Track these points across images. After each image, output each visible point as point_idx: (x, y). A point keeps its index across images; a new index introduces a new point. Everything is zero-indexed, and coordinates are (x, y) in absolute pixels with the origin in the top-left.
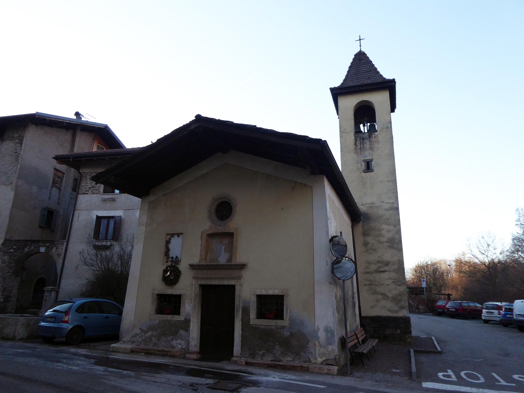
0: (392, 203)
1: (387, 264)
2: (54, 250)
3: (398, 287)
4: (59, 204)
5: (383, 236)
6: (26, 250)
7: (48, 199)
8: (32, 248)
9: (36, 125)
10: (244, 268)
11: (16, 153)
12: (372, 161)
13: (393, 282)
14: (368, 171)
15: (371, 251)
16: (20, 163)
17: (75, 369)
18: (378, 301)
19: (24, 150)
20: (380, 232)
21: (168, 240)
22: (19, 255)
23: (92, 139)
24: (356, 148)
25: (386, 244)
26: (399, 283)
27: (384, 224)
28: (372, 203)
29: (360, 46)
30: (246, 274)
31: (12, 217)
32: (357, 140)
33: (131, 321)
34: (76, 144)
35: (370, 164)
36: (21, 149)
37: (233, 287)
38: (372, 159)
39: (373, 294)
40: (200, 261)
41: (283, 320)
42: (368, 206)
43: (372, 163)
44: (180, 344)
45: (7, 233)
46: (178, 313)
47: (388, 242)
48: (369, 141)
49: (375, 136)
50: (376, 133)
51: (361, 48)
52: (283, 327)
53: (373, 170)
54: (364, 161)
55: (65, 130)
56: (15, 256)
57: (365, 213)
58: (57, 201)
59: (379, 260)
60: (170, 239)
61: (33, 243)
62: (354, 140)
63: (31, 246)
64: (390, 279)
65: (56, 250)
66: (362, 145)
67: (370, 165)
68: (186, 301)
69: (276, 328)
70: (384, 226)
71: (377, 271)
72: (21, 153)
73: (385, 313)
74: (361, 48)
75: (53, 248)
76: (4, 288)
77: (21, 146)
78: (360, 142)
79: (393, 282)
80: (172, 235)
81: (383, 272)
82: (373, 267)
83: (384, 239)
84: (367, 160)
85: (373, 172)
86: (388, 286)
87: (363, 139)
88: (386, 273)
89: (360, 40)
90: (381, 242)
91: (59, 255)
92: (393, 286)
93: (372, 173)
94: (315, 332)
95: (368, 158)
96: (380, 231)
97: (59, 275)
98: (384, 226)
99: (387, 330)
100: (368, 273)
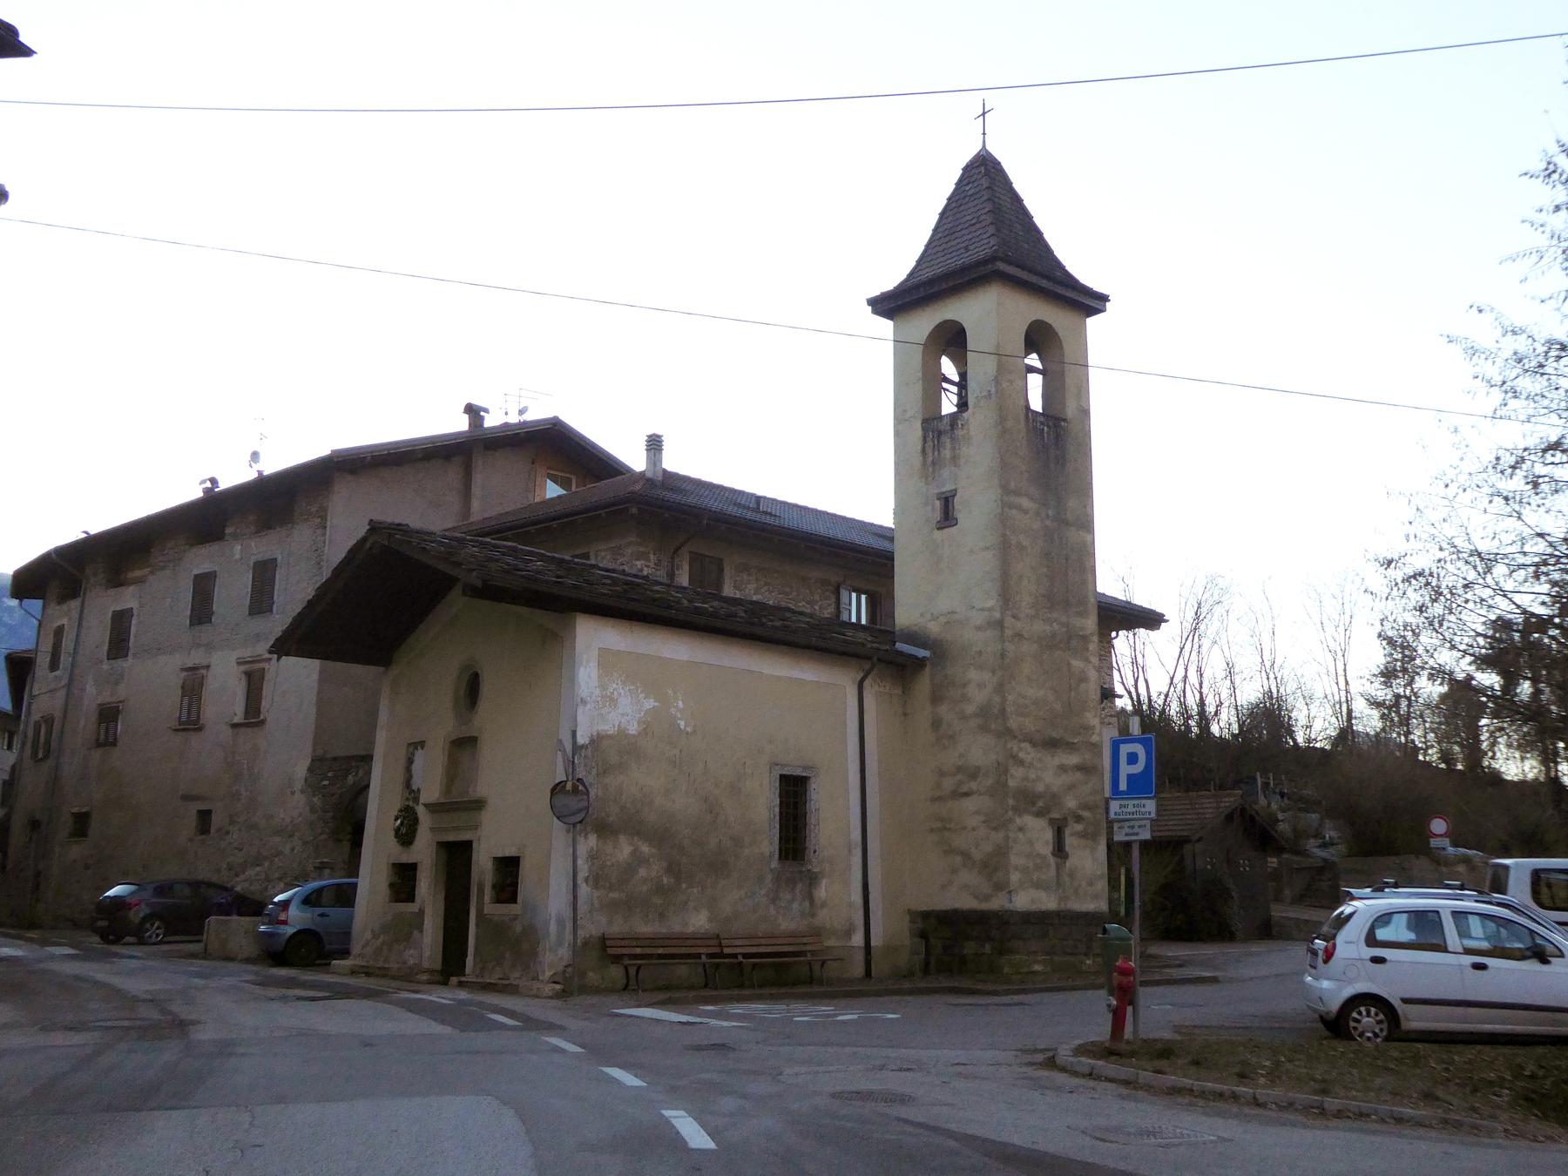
1: (974, 774)
14: (947, 523)
17: (60, 945)
18: (955, 871)
24: (924, 464)
29: (984, 134)
30: (486, 817)
31: (322, 704)
34: (476, 490)
36: (324, 543)
38: (956, 490)
39: (946, 853)
45: (316, 742)
46: (413, 901)
48: (951, 437)
51: (984, 142)
52: (516, 917)
60: (413, 754)
62: (922, 439)
63: (358, 771)
66: (936, 453)
70: (973, 675)
72: (326, 552)
73: (966, 903)
74: (984, 142)
77: (324, 534)
78: (934, 442)
79: (984, 822)
81: (966, 794)
82: (948, 784)
83: (970, 709)
85: (956, 524)
87: (940, 434)
90: (964, 718)
95: (948, 487)
96: (965, 685)
98: (973, 675)
100: (939, 799)
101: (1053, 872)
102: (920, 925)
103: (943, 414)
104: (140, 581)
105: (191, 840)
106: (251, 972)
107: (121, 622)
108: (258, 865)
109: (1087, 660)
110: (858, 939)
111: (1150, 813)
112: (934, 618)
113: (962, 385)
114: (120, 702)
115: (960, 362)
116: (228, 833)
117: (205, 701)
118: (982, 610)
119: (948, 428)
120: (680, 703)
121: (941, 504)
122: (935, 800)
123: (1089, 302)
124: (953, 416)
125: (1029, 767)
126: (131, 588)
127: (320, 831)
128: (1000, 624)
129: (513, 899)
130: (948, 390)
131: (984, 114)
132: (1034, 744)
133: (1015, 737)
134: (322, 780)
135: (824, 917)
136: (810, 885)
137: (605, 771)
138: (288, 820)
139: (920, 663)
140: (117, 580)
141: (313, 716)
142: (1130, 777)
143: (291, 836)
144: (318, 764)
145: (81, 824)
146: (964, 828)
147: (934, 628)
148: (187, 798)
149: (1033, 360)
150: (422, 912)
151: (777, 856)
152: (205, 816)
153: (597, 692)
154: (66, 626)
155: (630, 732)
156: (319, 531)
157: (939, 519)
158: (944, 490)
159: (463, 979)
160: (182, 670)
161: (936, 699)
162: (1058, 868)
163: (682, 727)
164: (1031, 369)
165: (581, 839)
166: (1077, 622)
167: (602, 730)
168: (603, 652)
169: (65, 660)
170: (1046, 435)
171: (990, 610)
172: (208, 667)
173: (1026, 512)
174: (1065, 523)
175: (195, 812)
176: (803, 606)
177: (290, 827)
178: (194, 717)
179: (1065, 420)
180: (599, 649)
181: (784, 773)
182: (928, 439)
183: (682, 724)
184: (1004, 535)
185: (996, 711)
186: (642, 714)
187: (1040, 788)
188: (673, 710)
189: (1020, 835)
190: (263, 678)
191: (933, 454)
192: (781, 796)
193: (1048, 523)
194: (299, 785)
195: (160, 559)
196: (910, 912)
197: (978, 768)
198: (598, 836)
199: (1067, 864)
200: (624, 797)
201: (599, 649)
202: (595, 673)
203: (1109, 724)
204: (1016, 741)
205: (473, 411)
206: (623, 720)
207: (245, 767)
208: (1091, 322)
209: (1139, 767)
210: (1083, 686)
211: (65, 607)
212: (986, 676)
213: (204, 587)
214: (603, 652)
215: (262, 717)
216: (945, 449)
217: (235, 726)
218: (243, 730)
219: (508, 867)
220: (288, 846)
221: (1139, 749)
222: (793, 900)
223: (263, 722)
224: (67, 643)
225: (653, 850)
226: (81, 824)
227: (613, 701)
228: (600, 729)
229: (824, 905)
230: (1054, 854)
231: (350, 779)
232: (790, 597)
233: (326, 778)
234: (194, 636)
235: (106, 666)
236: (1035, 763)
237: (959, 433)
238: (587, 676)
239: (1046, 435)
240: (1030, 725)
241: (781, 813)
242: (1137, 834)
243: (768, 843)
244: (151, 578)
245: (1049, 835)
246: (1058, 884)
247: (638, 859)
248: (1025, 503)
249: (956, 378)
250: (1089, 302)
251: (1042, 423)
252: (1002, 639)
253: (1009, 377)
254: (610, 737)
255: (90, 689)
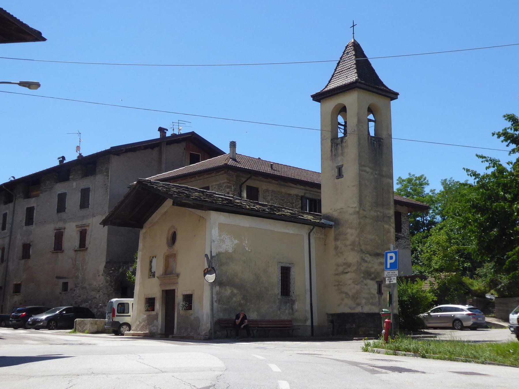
1: (349, 265)
18: (343, 300)
24: (332, 155)
29: (353, 33)
30: (180, 280)
38: (343, 165)
52: (192, 315)
60: (152, 260)
62: (331, 146)
63: (123, 267)
66: (336, 151)
73: (347, 310)
81: (347, 273)
82: (341, 269)
83: (348, 243)
85: (343, 177)
87: (337, 144)
90: (346, 246)
95: (340, 164)
96: (346, 235)
98: (349, 231)
101: (377, 299)
102: (331, 318)
103: (338, 137)
104: (37, 196)
105: (60, 293)
106: (509, 114)
107: (30, 211)
108: (87, 302)
109: (390, 225)
110: (309, 323)
111: (396, 274)
112: (335, 211)
113: (345, 126)
115: (345, 118)
117: (64, 242)
118: (352, 208)
119: (340, 142)
120: (246, 241)
121: (337, 170)
122: (336, 275)
123: (393, 95)
124: (342, 138)
125: (369, 263)
126: (34, 199)
128: (358, 213)
129: (191, 309)
130: (340, 128)
131: (353, 26)
132: (370, 255)
133: (364, 252)
135: (297, 315)
136: (292, 304)
137: (221, 265)
138: (97, 286)
139: (330, 226)
140: (27, 196)
141: (106, 247)
142: (391, 264)
143: (99, 291)
144: (109, 263)
145: (17, 289)
146: (346, 284)
147: (335, 214)
148: (58, 278)
149: (371, 117)
150: (157, 315)
151: (280, 294)
152: (65, 285)
153: (218, 238)
154: (8, 213)
155: (230, 251)
157: (337, 175)
158: (339, 165)
159: (173, 335)
161: (336, 239)
162: (379, 298)
163: (247, 250)
164: (370, 120)
165: (214, 288)
166: (387, 212)
167: (220, 251)
168: (220, 224)
169: (8, 226)
170: (375, 145)
171: (355, 208)
172: (65, 228)
173: (367, 173)
174: (382, 176)
176: (289, 205)
177: (98, 288)
179: (382, 139)
180: (219, 223)
181: (282, 265)
182: (333, 146)
183: (247, 249)
184: (360, 181)
185: (357, 243)
186: (234, 245)
187: (373, 270)
188: (244, 244)
189: (365, 286)
191: (335, 152)
192: (281, 273)
193: (376, 176)
194: (101, 272)
195: (44, 187)
196: (327, 314)
197: (351, 264)
198: (219, 287)
199: (383, 297)
200: (228, 274)
201: (219, 223)
202: (217, 232)
203: (407, 248)
204: (364, 254)
205: (162, 130)
206: (227, 248)
208: (392, 102)
209: (393, 261)
210: (389, 234)
211: (6, 206)
213: (62, 198)
214: (220, 224)
215: (86, 247)
216: (339, 150)
217: (76, 251)
218: (79, 252)
219: (188, 299)
221: (393, 255)
222: (286, 309)
223: (87, 249)
224: (9, 219)
225: (238, 292)
226: (17, 289)
227: (223, 241)
228: (219, 250)
229: (297, 311)
230: (377, 293)
231: (121, 270)
232: (284, 201)
233: (112, 270)
235: (25, 228)
236: (371, 261)
237: (344, 144)
238: (215, 232)
239: (375, 145)
240: (369, 248)
241: (281, 279)
242: (393, 281)
243: (278, 290)
244: (41, 195)
245: (376, 287)
246: (379, 304)
247: (233, 295)
248: (368, 169)
249: (343, 124)
250: (393, 95)
251: (374, 140)
253: (363, 123)
254: (222, 253)
255: (19, 237)
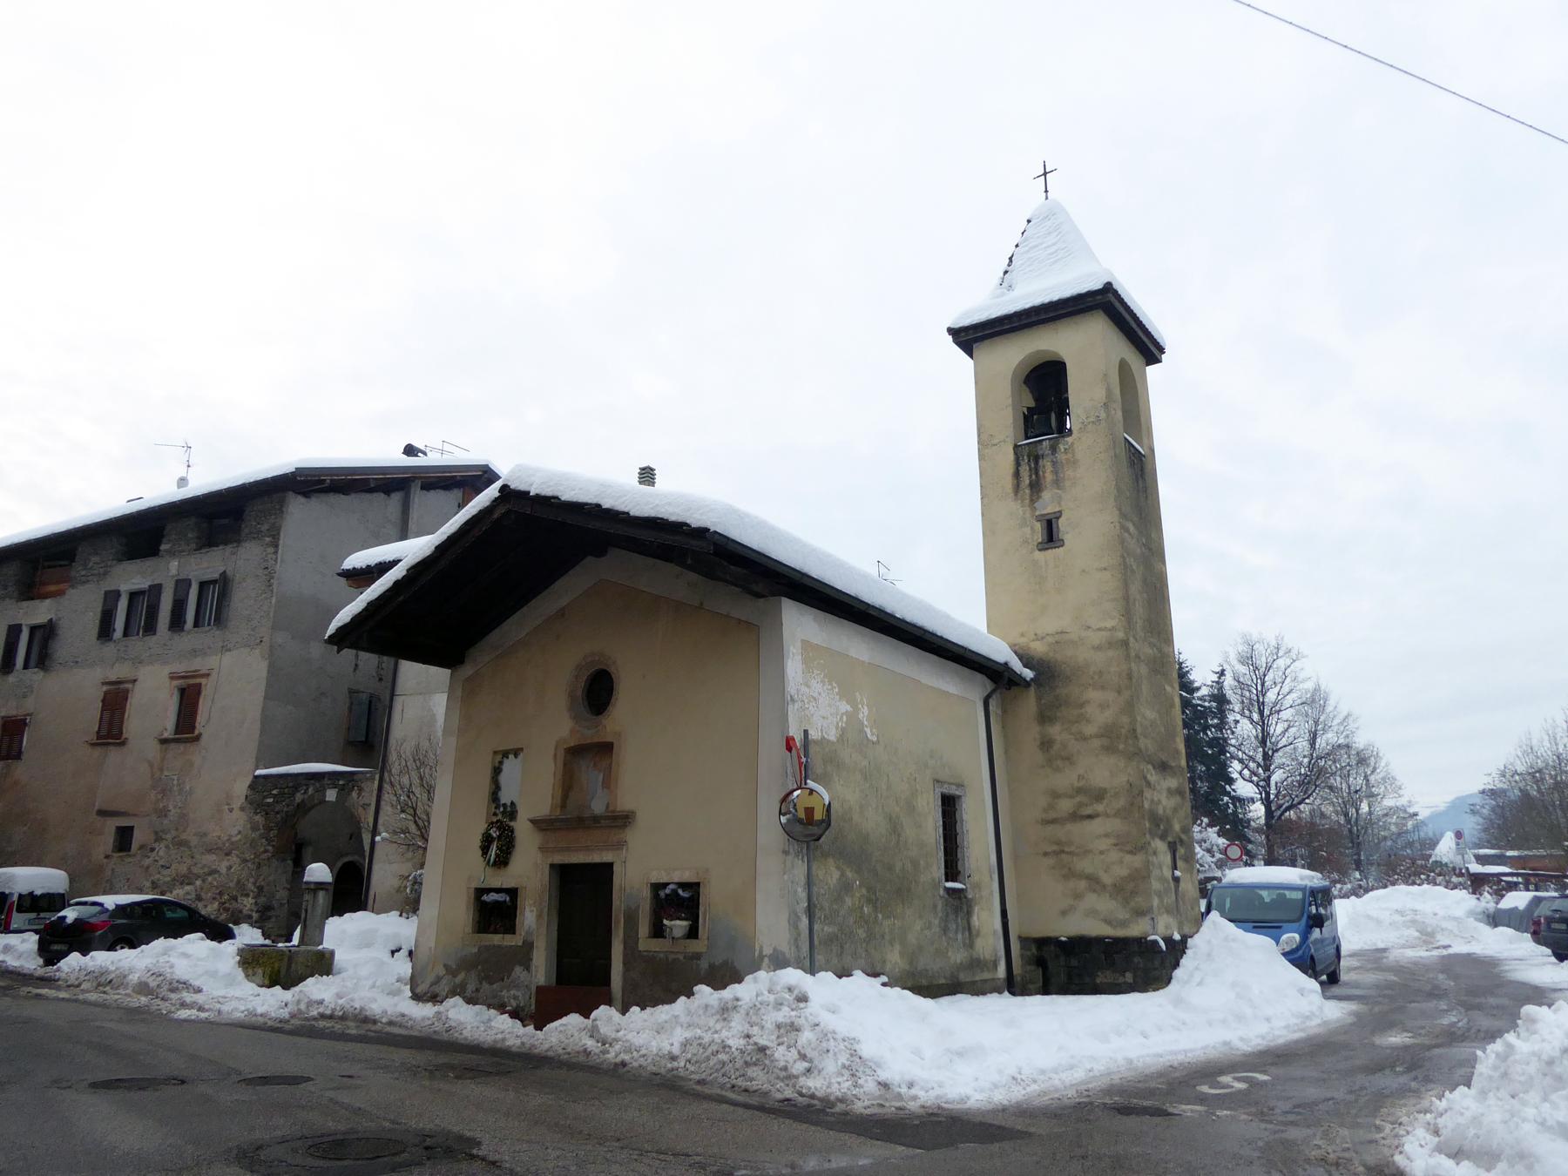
0: (1110, 630)
1: (1099, 795)
2: (354, 794)
3: (1128, 858)
4: (381, 679)
5: (1088, 721)
6: (299, 797)
7: (352, 670)
8: (311, 791)
9: (306, 494)
10: (630, 823)
11: (267, 568)
12: (1058, 518)
13: (1116, 845)
14: (1051, 544)
15: (1059, 762)
16: (275, 590)
18: (1078, 896)
19: (282, 561)
20: (1083, 710)
21: (497, 765)
22: (285, 809)
23: (457, 504)
25: (1096, 743)
26: (1128, 848)
27: (1090, 689)
28: (1062, 632)
29: (1046, 191)
30: (635, 837)
31: (266, 720)
32: (1022, 463)
33: (430, 948)
35: (1054, 526)
36: (276, 561)
37: (608, 867)
38: (1060, 512)
39: (1066, 877)
40: (551, 811)
41: (514, 933)
42: (1050, 639)
43: (1060, 521)
44: (515, 998)
46: (511, 929)
47: (1102, 736)
49: (1066, 447)
50: (1069, 439)
53: (1063, 540)
54: (1039, 518)
55: (382, 495)
56: (278, 813)
57: (1044, 661)
58: (374, 674)
59: (1081, 784)
60: (501, 763)
61: (312, 782)
63: (307, 789)
64: (1107, 835)
65: (359, 795)
67: (1055, 530)
68: (527, 903)
69: (685, 958)
70: (1093, 695)
71: (1075, 817)
73: (1094, 928)
75: (352, 791)
76: (258, 888)
77: (276, 553)
79: (1116, 845)
80: (505, 754)
81: (1090, 817)
82: (1066, 806)
83: (1089, 730)
84: (1048, 514)
85: (1062, 546)
86: (1103, 857)
88: (1097, 821)
89: (1045, 174)
91: (365, 806)
92: (1114, 855)
93: (1061, 548)
94: (1351, 1013)
96: (1082, 706)
97: (367, 854)
98: (1093, 695)
99: (1099, 973)
100: (1053, 821)
108: (188, 884)
112: (1038, 638)
114: (28, 715)
116: (152, 850)
118: (1099, 629)
126: (48, 601)
127: (262, 849)
128: (1125, 643)
134: (265, 797)
148: (102, 813)
150: (528, 946)
156: (271, 550)
160: (103, 684)
161: (1044, 718)
168: (806, 644)
171: (1113, 629)
175: (114, 828)
178: (115, 731)
190: (199, 693)
195: (83, 573)
207: (175, 782)
212: (1110, 696)
215: (197, 732)
217: (164, 741)
218: (173, 746)
220: (225, 864)
223: (198, 738)
234: (119, 650)
252: (1128, 657)
